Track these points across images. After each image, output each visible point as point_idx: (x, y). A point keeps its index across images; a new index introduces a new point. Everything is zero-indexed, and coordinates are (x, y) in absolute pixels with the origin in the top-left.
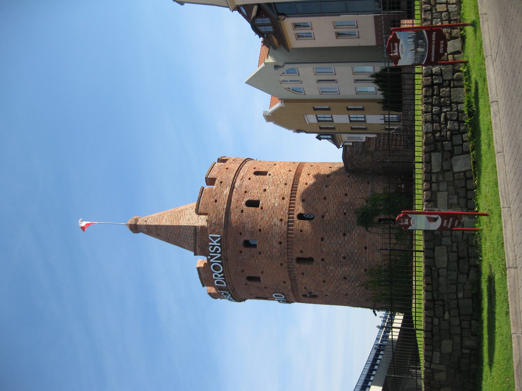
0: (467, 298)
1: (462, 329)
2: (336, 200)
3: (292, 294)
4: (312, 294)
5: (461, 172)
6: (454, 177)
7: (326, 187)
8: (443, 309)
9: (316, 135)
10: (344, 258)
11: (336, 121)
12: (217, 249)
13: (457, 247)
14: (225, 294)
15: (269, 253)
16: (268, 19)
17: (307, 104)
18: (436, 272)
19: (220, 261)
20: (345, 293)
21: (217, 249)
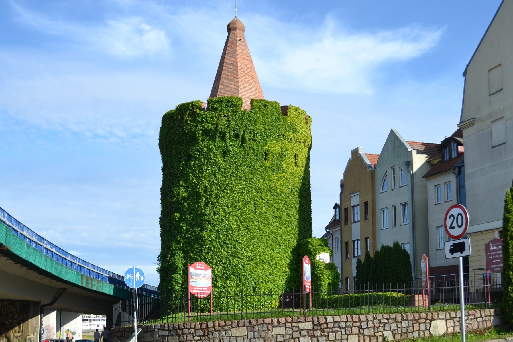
9: (338, 202)
11: (354, 226)
16: (456, 156)
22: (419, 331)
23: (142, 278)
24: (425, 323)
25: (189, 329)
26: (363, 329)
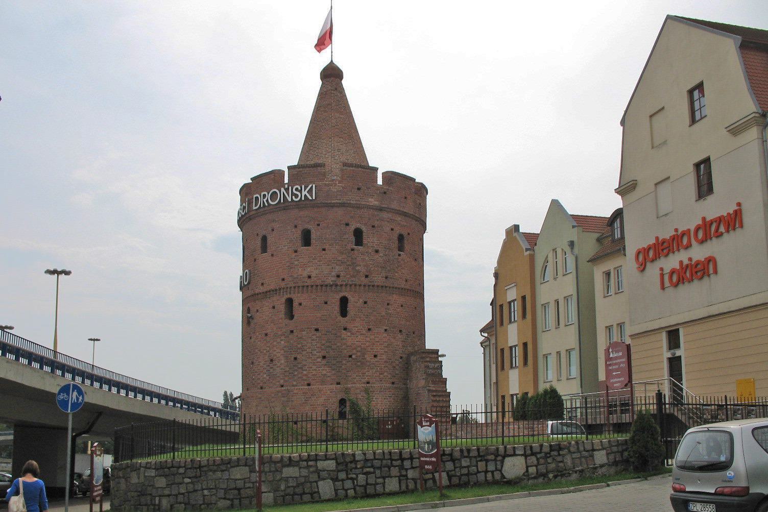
0: (204, 498)
1: (176, 495)
2: (367, 344)
3: (250, 295)
4: (250, 320)
5: (318, 489)
6: (314, 482)
7: (386, 330)
8: (192, 477)
10: (295, 359)
12: (296, 196)
13: (249, 488)
14: (244, 208)
15: (296, 263)
18: (225, 469)
19: (282, 201)
20: (254, 361)
21: (296, 196)
22: (486, 472)
23: (81, 398)
24: (495, 460)
25: (381, 460)
26: (406, 470)
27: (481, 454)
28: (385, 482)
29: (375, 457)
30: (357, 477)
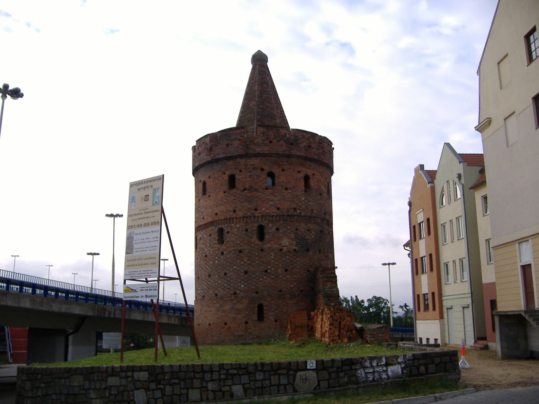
10: (225, 274)
13: (83, 394)
17: (431, 211)
24: (287, 374)
26: (207, 382)
27: (274, 368)
28: (188, 393)
29: (180, 369)
30: (165, 387)
